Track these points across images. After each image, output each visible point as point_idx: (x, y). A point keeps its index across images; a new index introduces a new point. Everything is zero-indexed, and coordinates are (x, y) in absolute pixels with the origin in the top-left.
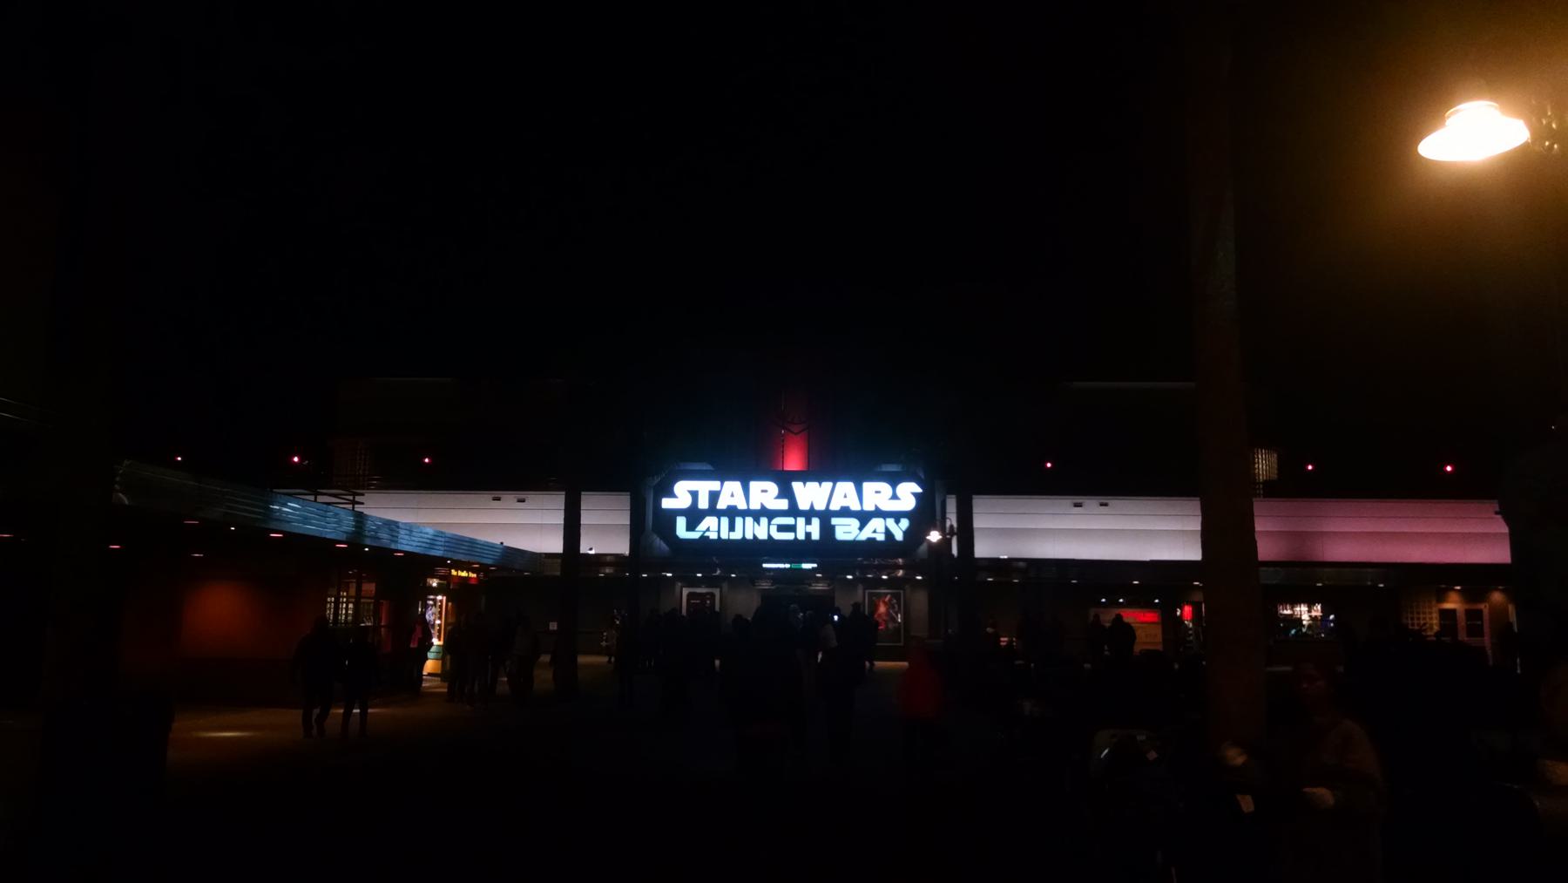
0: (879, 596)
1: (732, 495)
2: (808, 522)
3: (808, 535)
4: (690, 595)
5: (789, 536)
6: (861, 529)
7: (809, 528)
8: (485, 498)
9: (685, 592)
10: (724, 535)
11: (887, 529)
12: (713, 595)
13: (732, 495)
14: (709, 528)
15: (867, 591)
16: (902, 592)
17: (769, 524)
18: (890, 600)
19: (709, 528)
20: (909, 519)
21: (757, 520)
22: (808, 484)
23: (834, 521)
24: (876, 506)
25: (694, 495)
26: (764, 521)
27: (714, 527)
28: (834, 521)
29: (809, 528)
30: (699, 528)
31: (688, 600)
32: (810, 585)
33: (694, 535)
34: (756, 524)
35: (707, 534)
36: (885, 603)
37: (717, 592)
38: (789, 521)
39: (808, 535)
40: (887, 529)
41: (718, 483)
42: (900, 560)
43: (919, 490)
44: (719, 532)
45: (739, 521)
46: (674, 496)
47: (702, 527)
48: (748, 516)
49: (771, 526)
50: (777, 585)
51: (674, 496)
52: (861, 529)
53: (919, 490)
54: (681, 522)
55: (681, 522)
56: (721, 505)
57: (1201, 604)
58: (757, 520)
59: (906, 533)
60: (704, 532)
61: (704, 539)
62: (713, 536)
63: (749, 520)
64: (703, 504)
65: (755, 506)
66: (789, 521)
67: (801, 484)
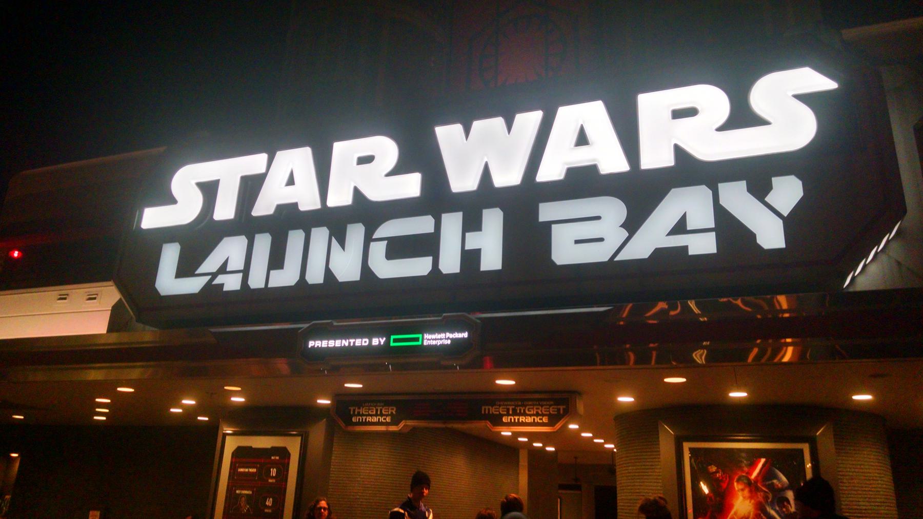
0: (730, 460)
1: (291, 182)
2: (472, 224)
3: (471, 258)
4: (241, 454)
5: (419, 267)
6: (632, 225)
7: (474, 241)
8: (51, 294)
9: (231, 445)
10: (257, 281)
11: (721, 214)
12: (284, 453)
13: (291, 182)
14: (225, 264)
15: (687, 446)
16: (806, 448)
17: (369, 239)
18: (767, 475)
19: (225, 264)
20: (791, 489)
21: (339, 235)
22: (478, 125)
23: (547, 212)
24: (678, 149)
25: (209, 190)
26: (356, 233)
27: (237, 262)
28: (547, 212)
29: (474, 241)
30: (202, 269)
31: (233, 467)
32: (497, 420)
33: (192, 285)
34: (334, 242)
35: (219, 280)
36: (752, 487)
37: (293, 446)
38: (422, 225)
39: (471, 258)
40: (721, 214)
41: (263, 157)
42: (783, 301)
43: (825, 84)
44: (246, 272)
45: (295, 239)
46: (173, 201)
47: (210, 264)
48: (319, 224)
49: (372, 244)
50: (410, 423)
51: (173, 201)
52: (632, 225)
53: (825, 84)
54: (170, 255)
55: (170, 255)
56: (264, 207)
57: (760, 515)
58: (339, 235)
59: (791, 223)
60: (214, 275)
61: (212, 290)
62: (231, 283)
63: (320, 235)
64: (225, 210)
65: (340, 197)
66: (422, 225)
67: (458, 128)
